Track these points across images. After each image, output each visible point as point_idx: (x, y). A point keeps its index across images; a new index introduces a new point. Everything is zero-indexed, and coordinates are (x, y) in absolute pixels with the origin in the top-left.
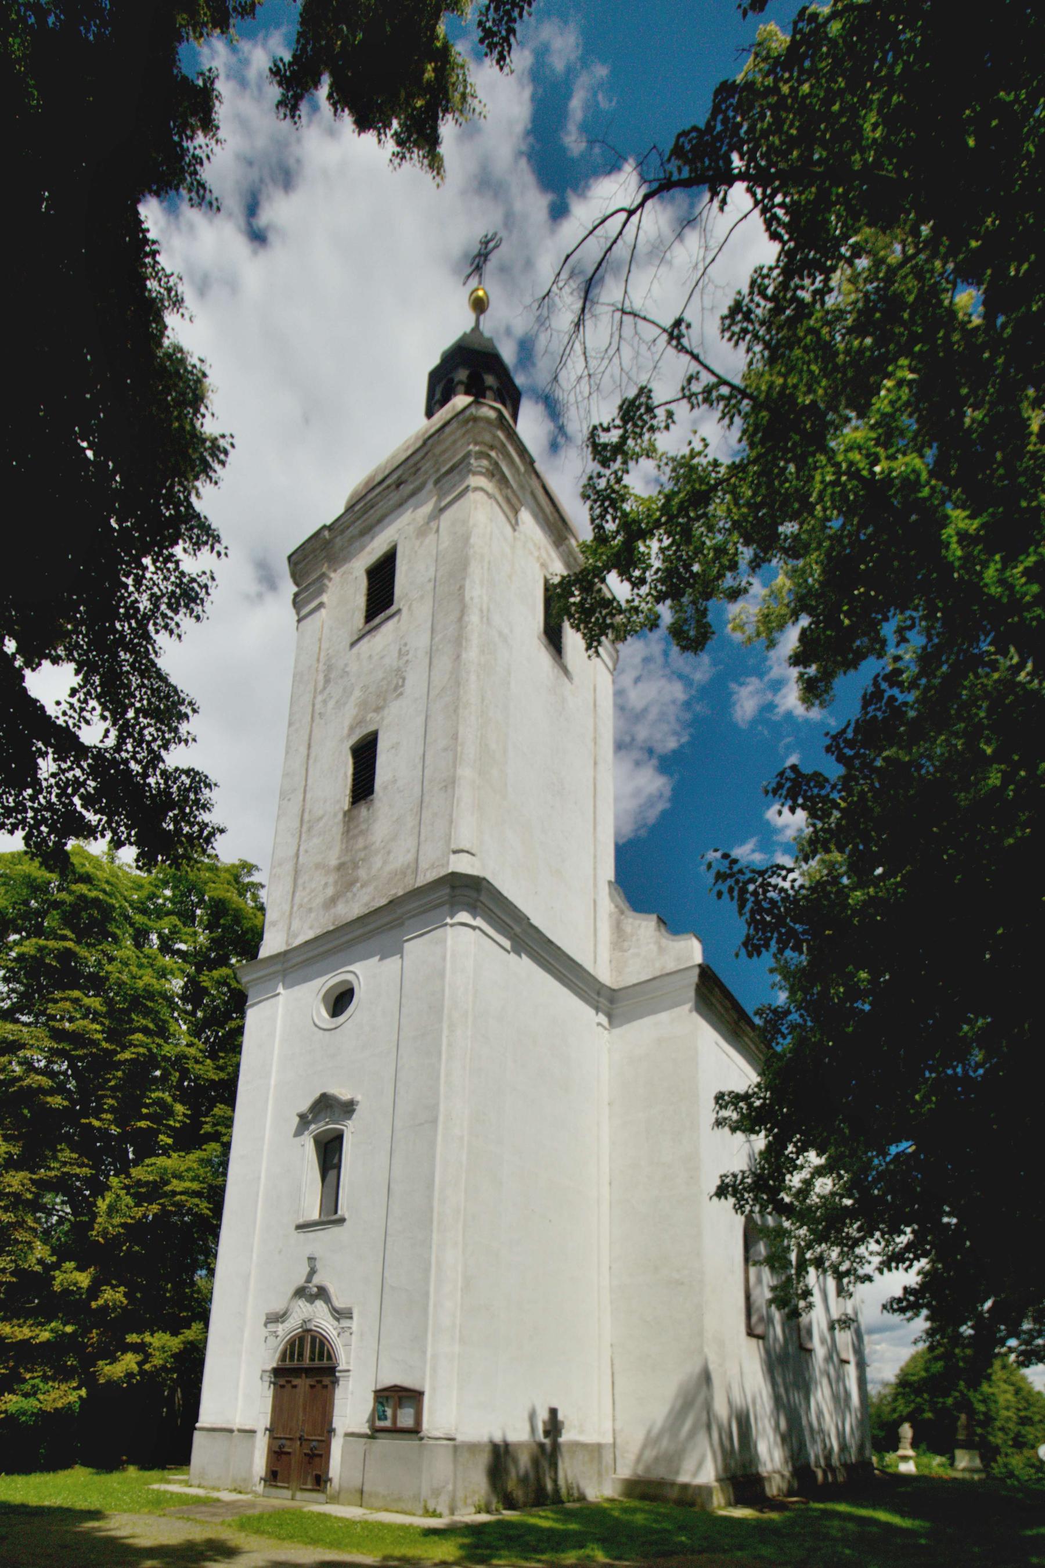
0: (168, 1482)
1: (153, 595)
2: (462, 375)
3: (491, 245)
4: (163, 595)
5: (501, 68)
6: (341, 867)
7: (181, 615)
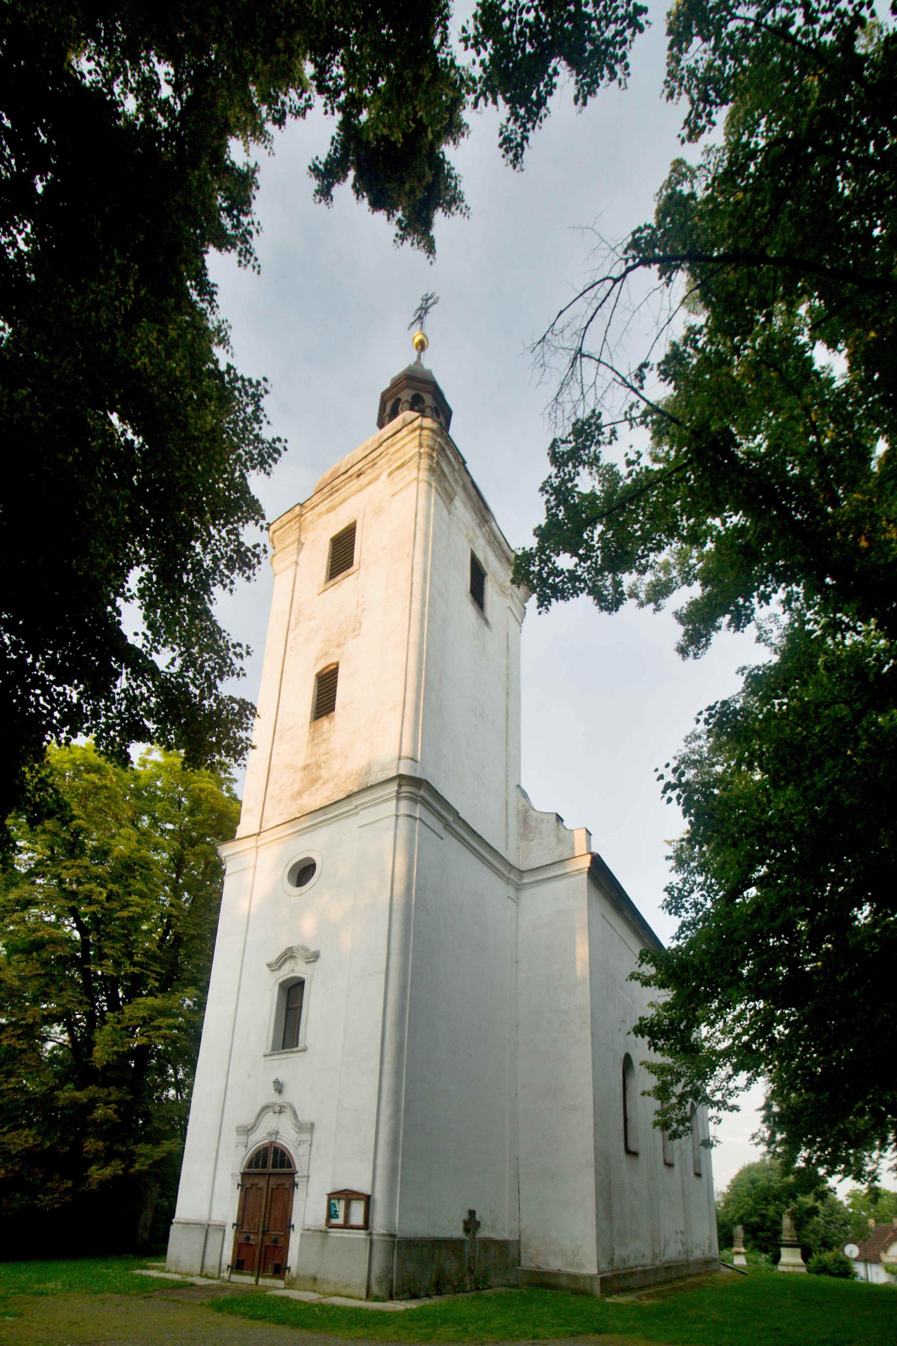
0: (147, 1268)
1: (215, 557)
2: (406, 395)
3: (431, 302)
4: (223, 558)
5: (515, 167)
6: (306, 767)
7: (235, 575)
